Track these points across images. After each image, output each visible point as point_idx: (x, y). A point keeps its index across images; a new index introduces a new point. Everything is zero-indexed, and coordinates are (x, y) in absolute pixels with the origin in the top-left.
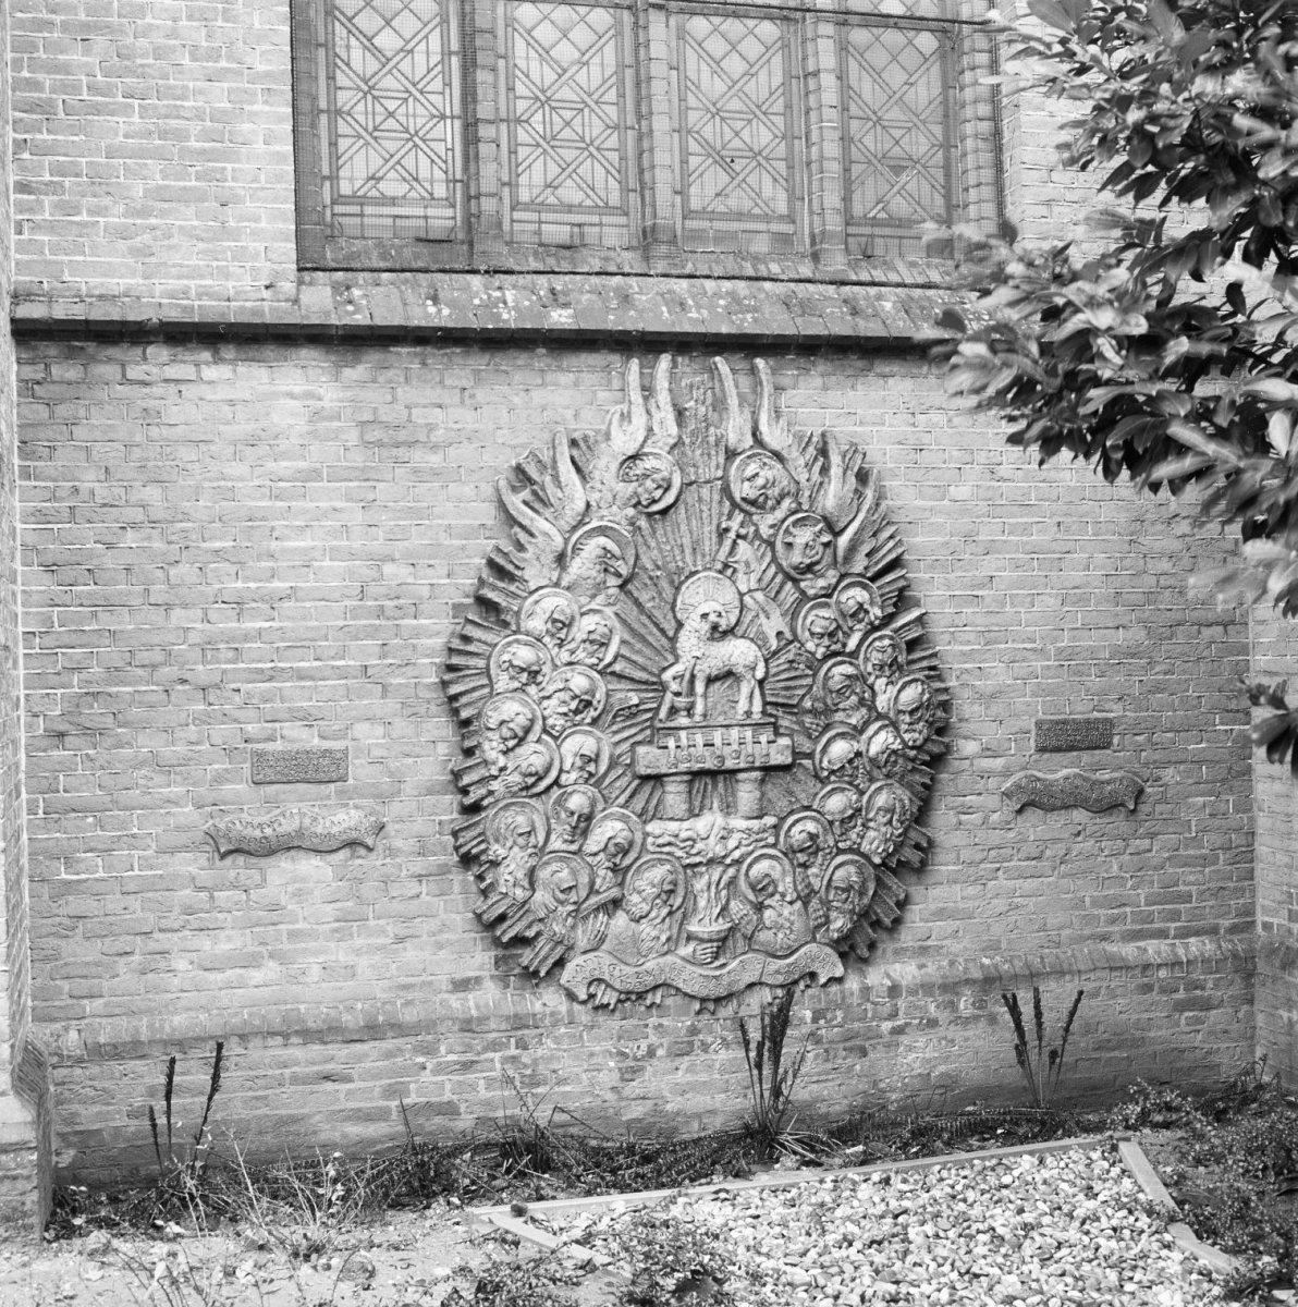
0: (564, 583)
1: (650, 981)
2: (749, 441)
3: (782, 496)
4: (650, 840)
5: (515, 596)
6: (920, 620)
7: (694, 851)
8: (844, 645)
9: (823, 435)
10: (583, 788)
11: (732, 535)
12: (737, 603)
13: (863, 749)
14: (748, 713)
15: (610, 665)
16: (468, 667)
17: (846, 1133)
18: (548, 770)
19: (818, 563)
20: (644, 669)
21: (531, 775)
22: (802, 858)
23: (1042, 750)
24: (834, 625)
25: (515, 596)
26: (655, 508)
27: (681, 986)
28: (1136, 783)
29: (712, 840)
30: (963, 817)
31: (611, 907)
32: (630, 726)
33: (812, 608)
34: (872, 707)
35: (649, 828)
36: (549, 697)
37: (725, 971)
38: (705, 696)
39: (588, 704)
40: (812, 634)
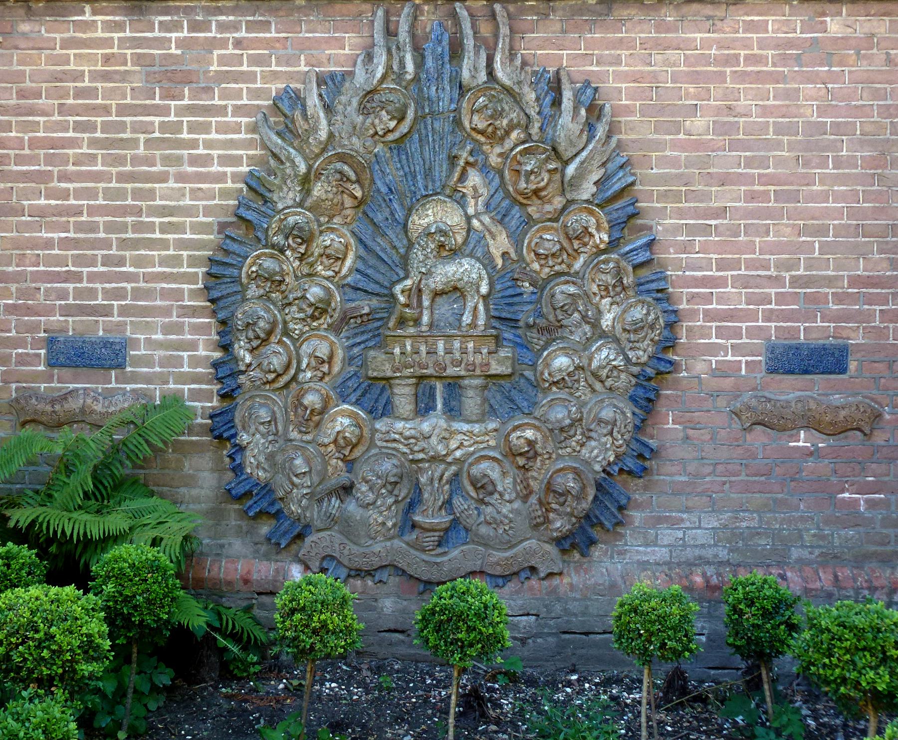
0: (308, 204)
1: (376, 562)
2: (483, 76)
3: (511, 127)
4: (378, 436)
5: (265, 215)
6: (650, 244)
7: (416, 448)
8: (569, 266)
9: (558, 72)
10: (318, 386)
11: (462, 162)
12: (463, 224)
13: (585, 362)
14: (473, 325)
15: (345, 277)
16: (224, 276)
17: (413, 34)
18: (288, 367)
19: (544, 188)
20: (377, 283)
21: (270, 372)
22: (521, 461)
23: (772, 371)
24: (558, 247)
25: (265, 215)
26: (391, 137)
27: (405, 568)
28: (873, 409)
29: (434, 440)
30: (691, 432)
31: (341, 492)
32: (363, 333)
33: (538, 231)
34: (595, 325)
35: (378, 425)
36: (290, 304)
37: (445, 559)
38: (431, 307)
39: (324, 311)
40: (537, 255)
